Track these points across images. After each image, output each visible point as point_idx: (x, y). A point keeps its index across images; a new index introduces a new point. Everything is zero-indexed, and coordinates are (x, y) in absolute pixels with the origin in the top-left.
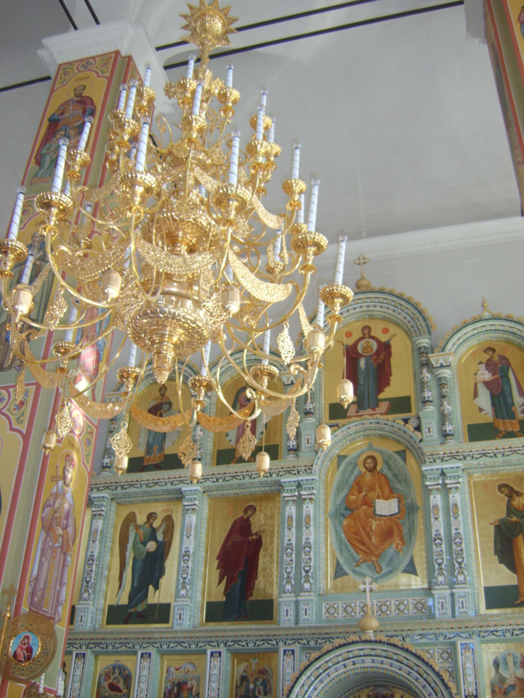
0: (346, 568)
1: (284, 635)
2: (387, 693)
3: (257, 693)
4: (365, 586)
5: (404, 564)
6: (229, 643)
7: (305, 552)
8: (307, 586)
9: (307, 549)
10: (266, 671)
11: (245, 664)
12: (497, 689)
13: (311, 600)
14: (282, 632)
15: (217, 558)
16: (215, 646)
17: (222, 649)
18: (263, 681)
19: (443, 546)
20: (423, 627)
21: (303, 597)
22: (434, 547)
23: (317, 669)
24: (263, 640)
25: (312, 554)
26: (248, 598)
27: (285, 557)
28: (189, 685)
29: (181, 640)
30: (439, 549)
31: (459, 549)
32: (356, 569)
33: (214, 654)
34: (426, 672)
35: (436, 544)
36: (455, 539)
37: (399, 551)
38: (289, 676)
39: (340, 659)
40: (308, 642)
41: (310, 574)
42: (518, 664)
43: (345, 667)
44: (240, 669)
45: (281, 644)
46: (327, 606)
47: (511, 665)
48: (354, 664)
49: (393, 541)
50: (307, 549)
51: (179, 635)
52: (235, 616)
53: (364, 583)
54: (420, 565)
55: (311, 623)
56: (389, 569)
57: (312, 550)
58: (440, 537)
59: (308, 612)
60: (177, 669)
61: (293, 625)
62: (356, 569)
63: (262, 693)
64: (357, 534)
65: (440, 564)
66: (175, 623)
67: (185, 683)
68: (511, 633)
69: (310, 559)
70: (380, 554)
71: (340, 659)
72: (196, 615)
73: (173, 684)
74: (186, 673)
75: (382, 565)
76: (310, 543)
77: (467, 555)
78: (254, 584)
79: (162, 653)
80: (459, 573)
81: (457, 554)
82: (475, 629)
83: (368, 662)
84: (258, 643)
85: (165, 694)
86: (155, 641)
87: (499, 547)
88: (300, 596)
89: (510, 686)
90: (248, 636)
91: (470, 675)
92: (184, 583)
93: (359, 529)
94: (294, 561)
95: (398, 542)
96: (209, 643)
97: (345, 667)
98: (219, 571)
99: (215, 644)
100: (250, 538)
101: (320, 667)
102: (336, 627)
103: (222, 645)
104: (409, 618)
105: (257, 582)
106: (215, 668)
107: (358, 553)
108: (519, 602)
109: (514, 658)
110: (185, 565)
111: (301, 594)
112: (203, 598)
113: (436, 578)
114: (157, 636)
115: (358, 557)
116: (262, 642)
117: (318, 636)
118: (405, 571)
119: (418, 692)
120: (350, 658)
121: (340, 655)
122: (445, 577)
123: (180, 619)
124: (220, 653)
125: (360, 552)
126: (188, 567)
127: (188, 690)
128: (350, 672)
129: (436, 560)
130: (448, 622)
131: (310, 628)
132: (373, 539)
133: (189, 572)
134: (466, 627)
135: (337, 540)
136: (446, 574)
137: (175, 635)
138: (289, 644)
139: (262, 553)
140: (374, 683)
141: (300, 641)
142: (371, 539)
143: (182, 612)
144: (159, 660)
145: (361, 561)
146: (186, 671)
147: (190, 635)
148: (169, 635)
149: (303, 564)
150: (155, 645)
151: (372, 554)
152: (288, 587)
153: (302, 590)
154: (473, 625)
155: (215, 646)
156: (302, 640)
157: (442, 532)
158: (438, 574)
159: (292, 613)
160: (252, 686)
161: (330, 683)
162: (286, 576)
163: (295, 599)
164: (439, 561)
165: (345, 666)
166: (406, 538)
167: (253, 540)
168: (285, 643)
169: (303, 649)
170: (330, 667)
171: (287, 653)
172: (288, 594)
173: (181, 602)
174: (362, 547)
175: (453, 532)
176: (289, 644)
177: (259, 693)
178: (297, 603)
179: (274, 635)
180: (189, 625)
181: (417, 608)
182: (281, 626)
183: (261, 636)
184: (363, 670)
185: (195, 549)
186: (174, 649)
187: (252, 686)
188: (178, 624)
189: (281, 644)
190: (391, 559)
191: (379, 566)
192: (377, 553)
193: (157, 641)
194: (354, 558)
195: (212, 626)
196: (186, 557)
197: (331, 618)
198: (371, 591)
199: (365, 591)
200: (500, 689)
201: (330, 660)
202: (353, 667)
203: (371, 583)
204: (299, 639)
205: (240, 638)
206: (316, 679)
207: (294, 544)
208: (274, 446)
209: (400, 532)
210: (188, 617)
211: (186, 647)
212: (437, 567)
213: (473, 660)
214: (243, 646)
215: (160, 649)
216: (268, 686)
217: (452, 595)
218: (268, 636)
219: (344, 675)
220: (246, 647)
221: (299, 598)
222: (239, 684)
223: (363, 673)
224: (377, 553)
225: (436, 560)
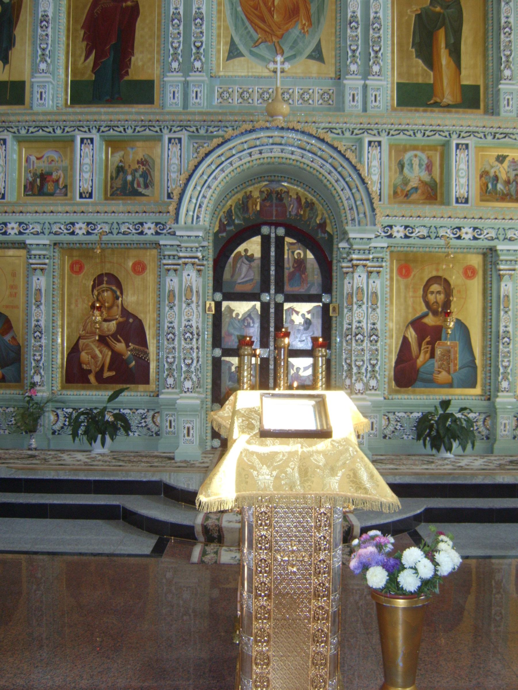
0: (242, 48)
1: (169, 121)
2: (281, 190)
3: (135, 186)
4: (275, 66)
5: (309, 50)
6: (102, 129)
7: (196, 25)
8: (198, 64)
9: (198, 20)
10: (147, 161)
11: (121, 153)
12: (399, 191)
13: (203, 82)
14: (167, 117)
15: (82, 28)
16: (85, 132)
17: (95, 136)
18: (143, 172)
19: (359, 30)
20: (330, 120)
21: (193, 77)
22: (349, 31)
23: (219, 156)
24: (144, 126)
25: (204, 27)
26: (122, 78)
27: (171, 28)
28: (54, 176)
29: (43, 124)
30: (354, 34)
31: (376, 35)
32: (253, 49)
33: (85, 141)
34: (341, 165)
35: (351, 28)
36: (373, 24)
37: (304, 32)
38: (175, 166)
39: (246, 146)
40: (197, 130)
41: (202, 51)
42: (424, 167)
43: (251, 156)
44: (115, 159)
45: (165, 131)
46: (221, 91)
47: (416, 167)
48: (261, 153)
49: (298, 20)
50: (198, 20)
51: (41, 118)
52: (108, 98)
53: (275, 62)
54: (328, 52)
55: (203, 108)
56: (292, 53)
57: (205, 22)
58: (356, 20)
59: (199, 95)
60: (38, 159)
61: (181, 110)
62: (253, 49)
63: (142, 186)
64: (256, 9)
65: (354, 51)
66: (35, 102)
67: (50, 174)
68: (422, 134)
69: (202, 33)
70: (283, 35)
71: (246, 146)
72: (60, 96)
73: (35, 175)
74: (50, 163)
75: (284, 48)
76: (201, 13)
77: (384, 44)
78: (130, 60)
79: (20, 140)
80: (374, 63)
81: (374, 42)
82: (385, 126)
83: (276, 152)
84: (138, 129)
85: (25, 187)
86: (11, 125)
87: (417, 40)
88: (189, 76)
89: (412, 188)
90: (127, 121)
91: (375, 175)
92: (43, 55)
93: (259, 3)
94: (182, 35)
95: (304, 22)
96: (78, 128)
97: (251, 156)
98: (85, 43)
99: (86, 129)
100: (124, 4)
101: (222, 154)
102: (232, 114)
103: (94, 131)
104: (314, 109)
105: (133, 59)
106: (87, 156)
107: (256, 31)
108: (432, 102)
109: (420, 160)
110: (44, 33)
111: (190, 74)
112: (67, 76)
113: (347, 66)
114: (12, 118)
115: (256, 36)
116: (143, 129)
117: (209, 123)
118: (310, 57)
119: (330, 186)
120: (256, 146)
121: (246, 142)
122: (358, 66)
123: (41, 99)
124: (92, 140)
125: (259, 30)
126: (47, 35)
127: (53, 182)
128: (255, 162)
129: (350, 45)
130: (358, 116)
131: (201, 113)
132: (275, 17)
133: (50, 42)
134: (377, 124)
135: (232, 14)
136: (359, 62)
137: (35, 118)
138: (175, 132)
139: (139, 24)
140: (269, 178)
141: (188, 129)
142: (273, 17)
143: (43, 91)
144: (16, 147)
145: (260, 41)
146: (50, 160)
147: (54, 118)
148: (28, 118)
149: (193, 39)
150: (10, 129)
151: (273, 33)
152: (175, 65)
153: (192, 69)
154: (384, 121)
155: (85, 132)
156: (190, 127)
157: (359, 14)
158: (351, 62)
159: (179, 96)
160: (129, 178)
161: (232, 173)
162: (172, 51)
163: (183, 79)
164: (354, 47)
165: (250, 155)
166: (314, 19)
167: (127, 7)
168: (171, 130)
169: (190, 137)
170: (234, 155)
171: (173, 141)
172: (175, 74)
173: (39, 78)
174: (262, 25)
175: (372, 15)
176: (175, 132)
177: (139, 185)
178: (186, 84)
179: (158, 121)
180: (53, 107)
181: (323, 99)
182: (167, 110)
183: (142, 121)
184: (269, 160)
185: (54, 13)
186: (35, 134)
187: (129, 178)
188: (39, 105)
189: (165, 131)
190: (295, 42)
191: (281, 48)
192: (279, 33)
193: (13, 125)
194: (251, 37)
195: (78, 109)
196: (44, 23)
197: (225, 104)
198: (282, 71)
199: (275, 72)
200: (402, 191)
201: (234, 147)
202: (259, 156)
203: (283, 63)
204: (187, 126)
205: (116, 123)
206: (216, 168)
207: (182, 13)
208: (13, 83)
209: (308, 10)
210: (51, 97)
211: (50, 132)
212: (350, 54)
213: (380, 159)
214: (121, 132)
215: (17, 134)
216: (149, 178)
217: (365, 87)
218: (150, 121)
219: (248, 165)
220: (124, 134)
221: (188, 79)
222: (114, 175)
223: (269, 164)
224: (279, 33)
225: (350, 45)
